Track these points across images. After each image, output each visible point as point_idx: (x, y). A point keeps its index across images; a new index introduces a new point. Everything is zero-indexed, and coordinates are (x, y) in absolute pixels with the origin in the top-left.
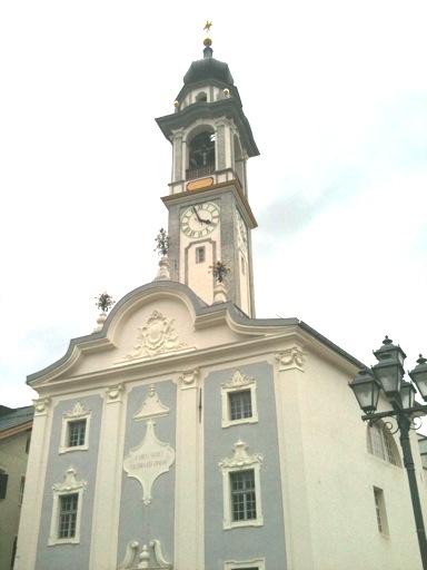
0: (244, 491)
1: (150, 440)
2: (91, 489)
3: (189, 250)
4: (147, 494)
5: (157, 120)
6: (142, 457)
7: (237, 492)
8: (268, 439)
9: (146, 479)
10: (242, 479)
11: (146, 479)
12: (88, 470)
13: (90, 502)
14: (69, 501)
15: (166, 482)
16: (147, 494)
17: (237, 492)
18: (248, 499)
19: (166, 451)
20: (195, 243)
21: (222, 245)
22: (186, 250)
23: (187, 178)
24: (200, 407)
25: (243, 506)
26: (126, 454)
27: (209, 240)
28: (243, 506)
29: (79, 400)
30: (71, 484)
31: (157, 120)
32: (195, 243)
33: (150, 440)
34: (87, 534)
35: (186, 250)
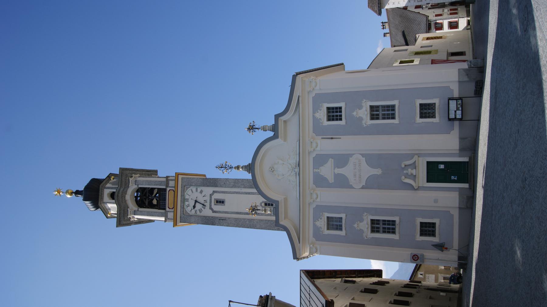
0: (381, 226)
1: (347, 171)
2: (368, 210)
3: (215, 210)
4: (378, 172)
5: (117, 227)
6: (355, 175)
7: (381, 230)
8: (355, 97)
9: (368, 171)
10: (375, 226)
11: (368, 171)
12: (356, 213)
13: (375, 211)
14: (375, 226)
15: (373, 159)
16: (378, 172)
17: (381, 230)
18: (426, 227)
19: (352, 160)
20: (210, 206)
21: (216, 186)
22: (214, 212)
23: (165, 209)
24: (332, 138)
25: (389, 112)
26: (351, 187)
27: (211, 195)
28: (389, 112)
29: (314, 221)
30: (365, 226)
31: (117, 227)
32: (210, 206)
33: (347, 171)
34: (392, 212)
35: (214, 212)
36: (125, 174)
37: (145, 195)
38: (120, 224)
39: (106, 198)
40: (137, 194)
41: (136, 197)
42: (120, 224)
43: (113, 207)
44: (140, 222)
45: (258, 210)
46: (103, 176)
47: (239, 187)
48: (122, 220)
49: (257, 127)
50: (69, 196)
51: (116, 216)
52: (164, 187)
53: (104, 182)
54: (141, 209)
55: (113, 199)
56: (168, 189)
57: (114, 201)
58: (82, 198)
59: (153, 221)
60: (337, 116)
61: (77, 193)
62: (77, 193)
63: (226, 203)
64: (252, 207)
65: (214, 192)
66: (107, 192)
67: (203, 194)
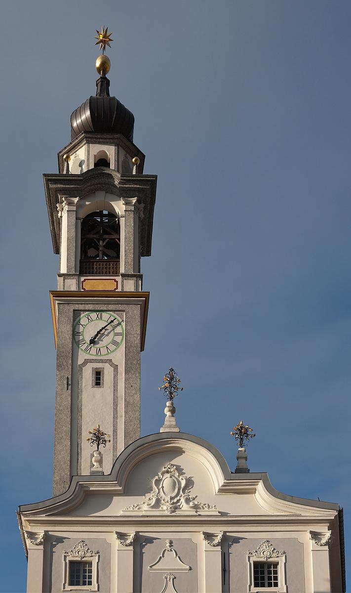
5: (45, 175)
20: (91, 361)
32: (91, 361)
36: (145, 192)
37: (106, 233)
38: (50, 179)
39: (97, 148)
40: (105, 216)
41: (100, 214)
42: (50, 179)
43: (81, 159)
44: (56, 224)
45: (98, 445)
46: (139, 139)
47: (126, 412)
48: (61, 185)
49: (245, 441)
50: (98, 63)
51: (65, 172)
52: (122, 270)
53: (128, 143)
54: (79, 222)
55: (96, 165)
56: (119, 279)
57: (92, 166)
58: (94, 95)
59: (57, 251)
60: (263, 578)
61: (104, 83)
62: (104, 83)
63: (98, 390)
64: (103, 434)
65: (116, 367)
66: (110, 151)
67: (112, 347)
